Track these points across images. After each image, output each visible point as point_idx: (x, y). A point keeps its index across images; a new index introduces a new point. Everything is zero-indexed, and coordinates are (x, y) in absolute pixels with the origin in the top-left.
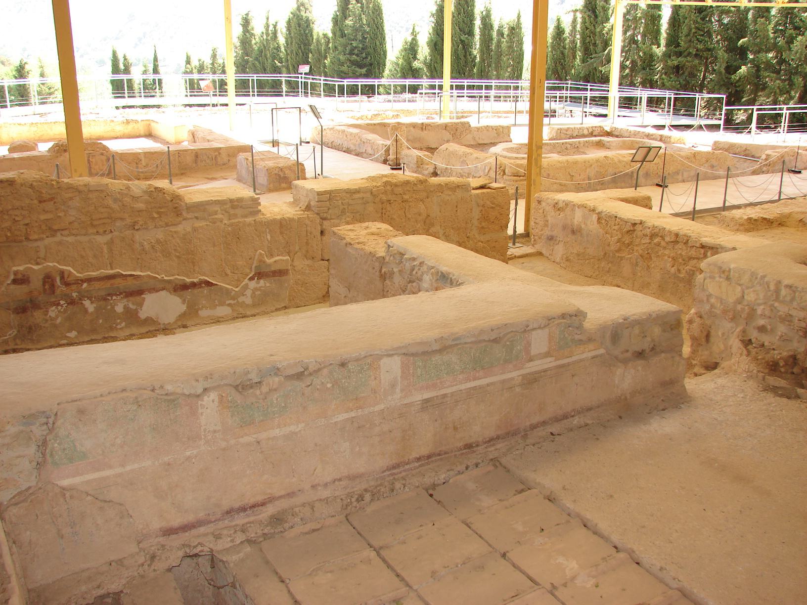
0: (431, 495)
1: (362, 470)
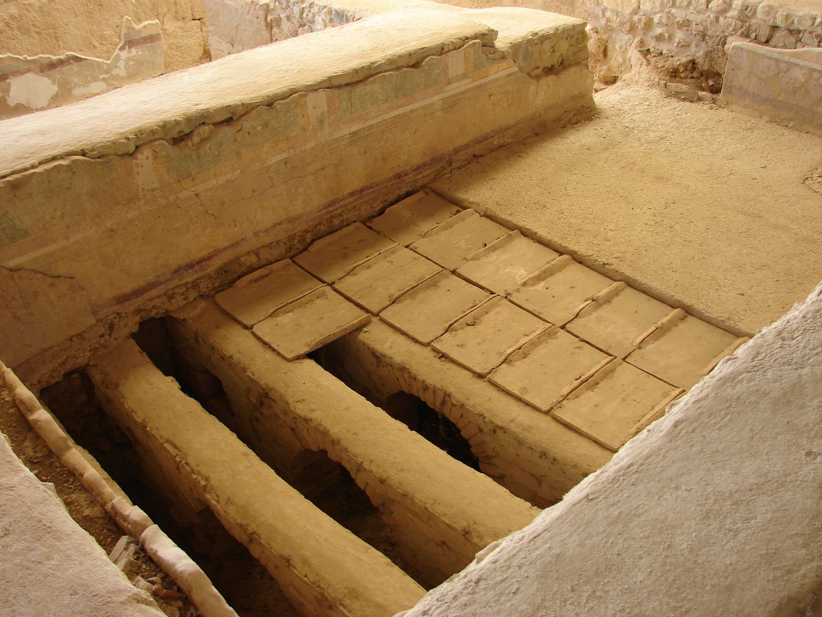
0: (370, 228)
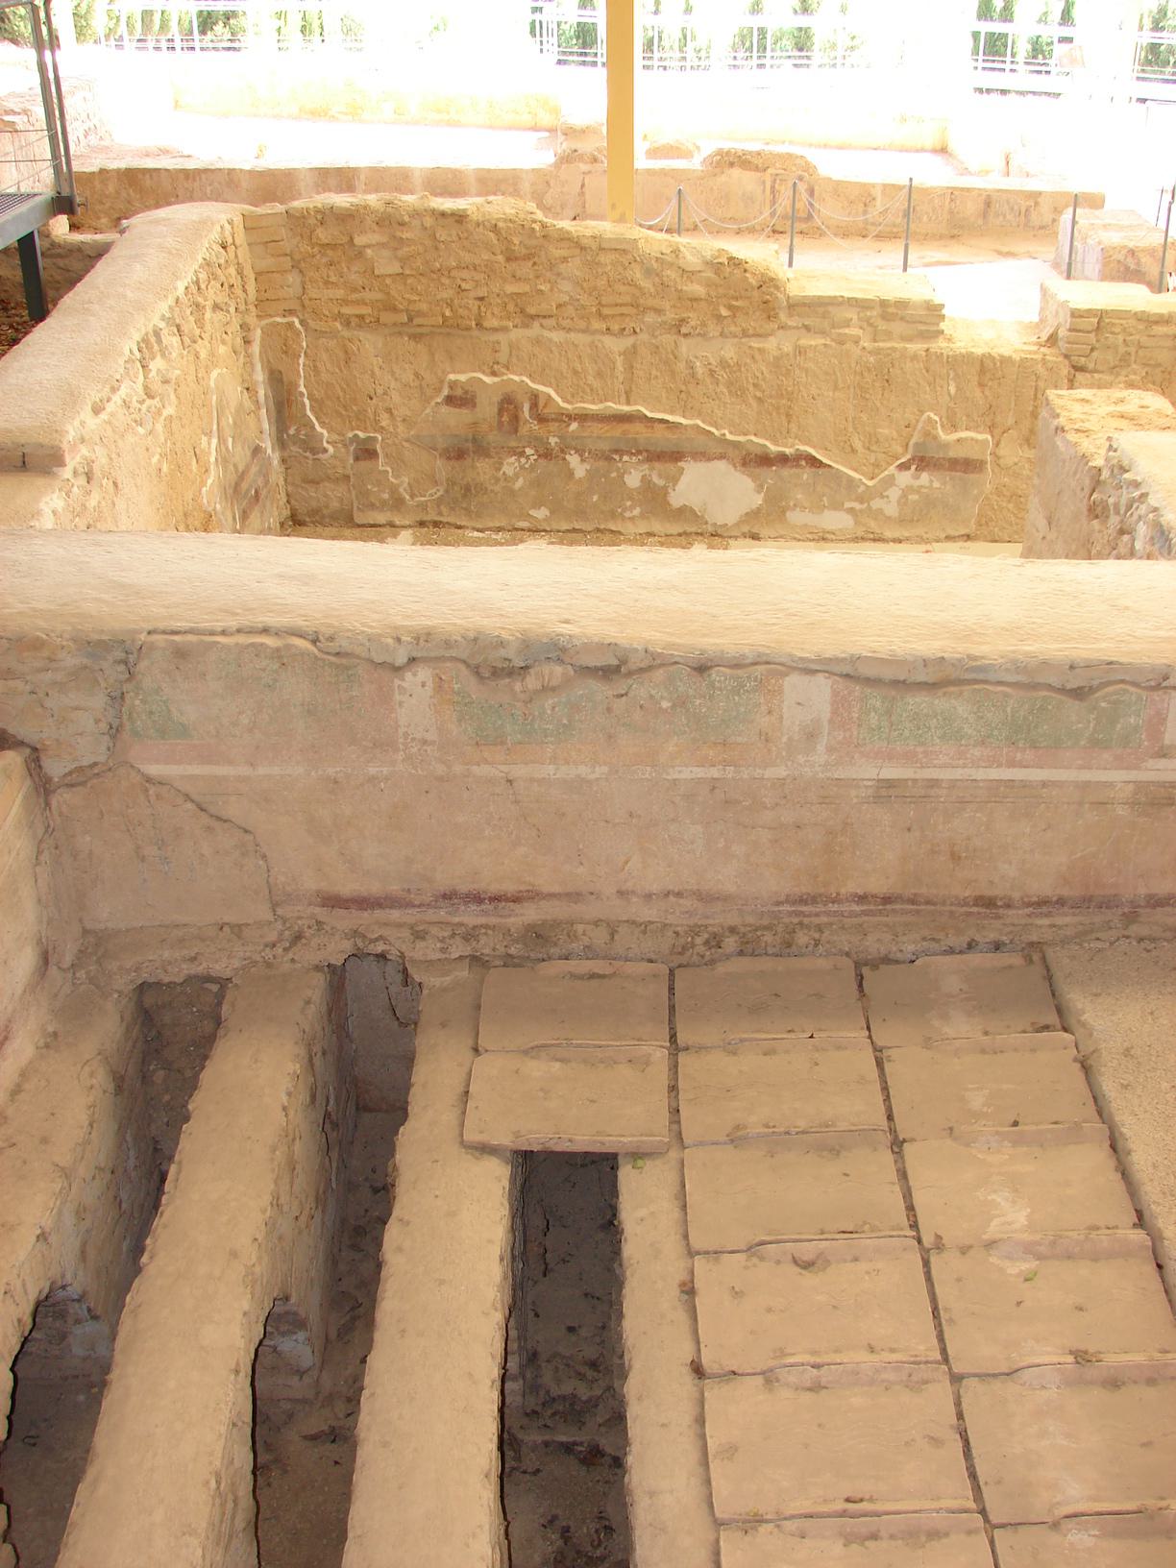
1: (730, 888)
